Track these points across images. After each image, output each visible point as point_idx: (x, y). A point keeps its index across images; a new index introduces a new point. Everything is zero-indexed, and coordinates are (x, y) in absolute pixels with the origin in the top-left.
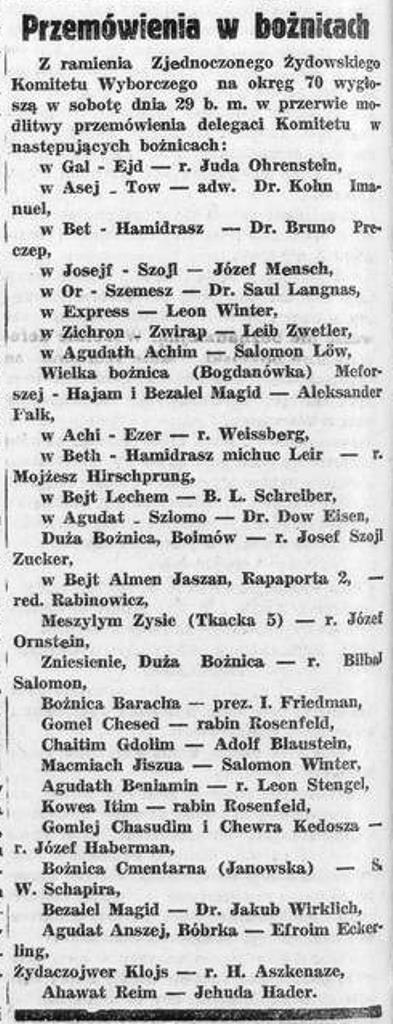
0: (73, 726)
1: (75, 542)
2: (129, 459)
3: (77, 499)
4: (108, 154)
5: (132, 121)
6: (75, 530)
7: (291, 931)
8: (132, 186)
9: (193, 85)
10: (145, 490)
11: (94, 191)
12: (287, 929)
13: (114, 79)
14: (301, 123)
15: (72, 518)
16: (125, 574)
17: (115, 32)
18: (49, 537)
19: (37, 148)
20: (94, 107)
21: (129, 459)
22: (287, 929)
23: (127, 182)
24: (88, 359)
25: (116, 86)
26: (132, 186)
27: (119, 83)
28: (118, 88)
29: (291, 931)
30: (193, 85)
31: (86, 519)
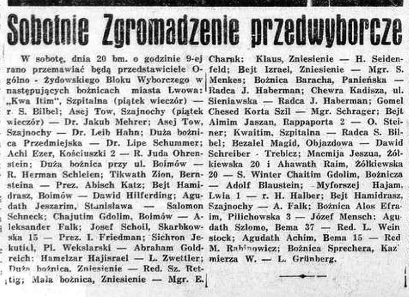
0: (187, 144)
1: (168, 134)
2: (374, 187)
3: (160, 186)
4: (150, 84)
5: (65, 194)
6: (234, 254)
7: (391, 207)
8: (98, 111)
9: (97, 81)
10: (385, 192)
11: (174, 124)
12: (389, 206)
13: (145, 77)
14: (390, 100)
15: (187, 195)
16: (217, 119)
17: (138, 23)
18: (44, 163)
19: (145, 70)
20: (181, 134)
21: (374, 187)
22: (389, 206)
23: (95, 109)
24: (255, 241)
25: (146, 81)
26: (98, 111)
27: (147, 79)
28: (147, 82)
29: (391, 207)
30: (97, 81)
31: (254, 239)
